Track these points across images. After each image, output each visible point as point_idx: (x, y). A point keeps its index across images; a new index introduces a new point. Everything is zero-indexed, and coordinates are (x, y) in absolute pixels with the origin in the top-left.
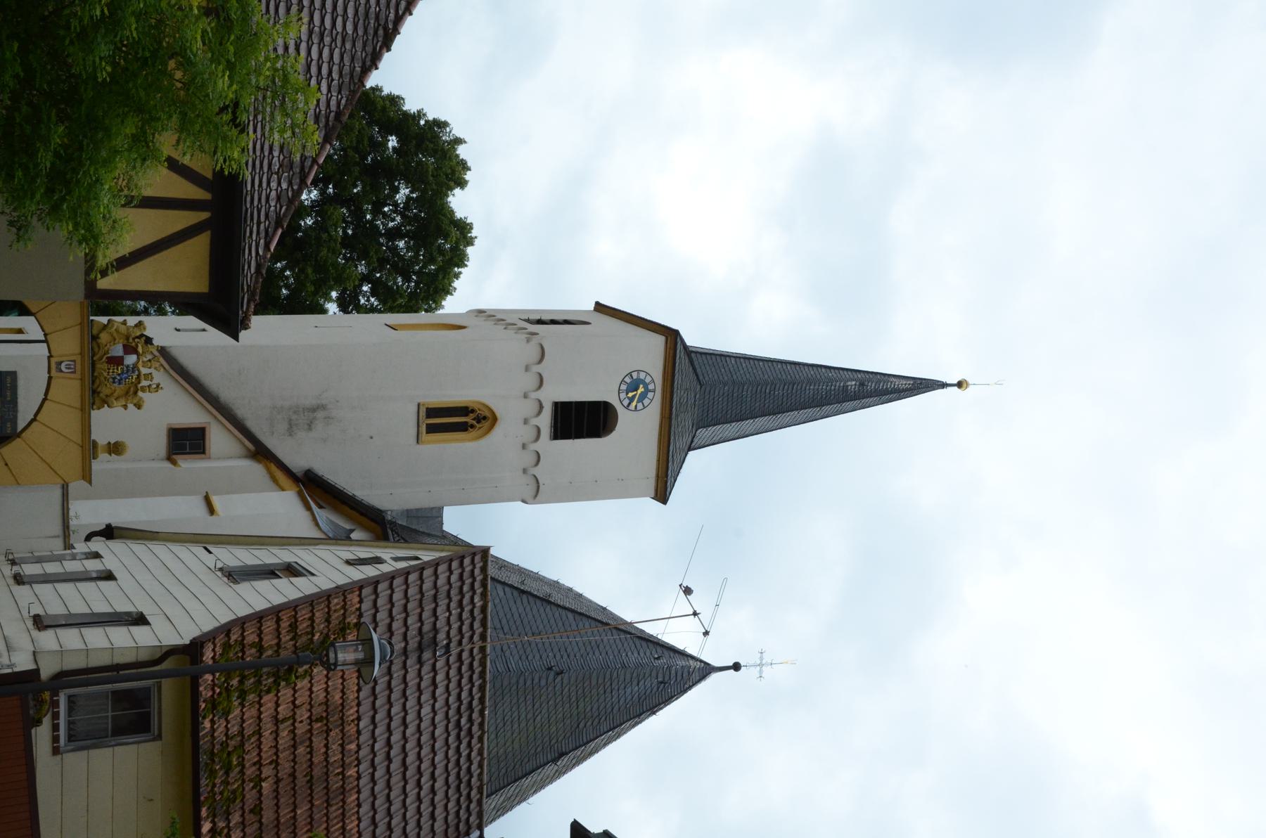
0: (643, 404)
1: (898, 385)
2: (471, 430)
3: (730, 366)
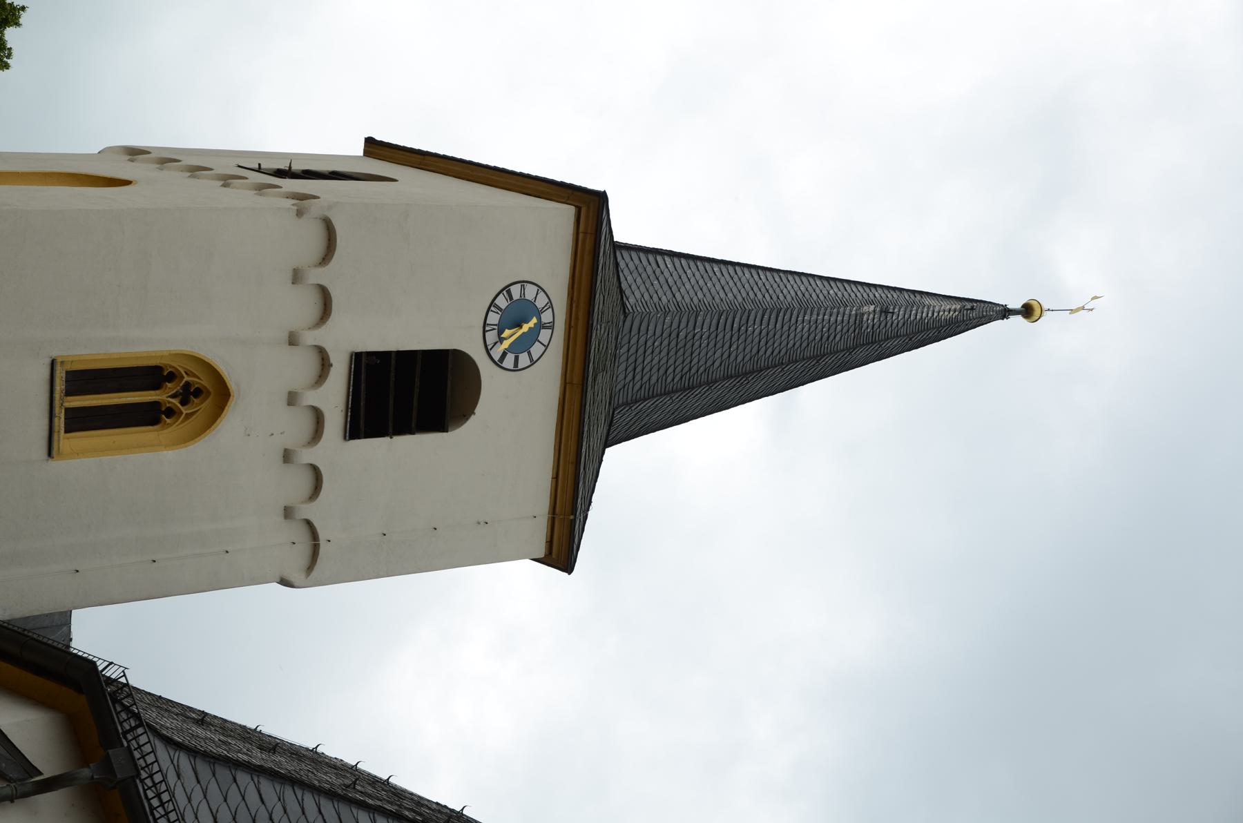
0: (529, 353)
1: (939, 312)
2: (168, 421)
3: (667, 274)
